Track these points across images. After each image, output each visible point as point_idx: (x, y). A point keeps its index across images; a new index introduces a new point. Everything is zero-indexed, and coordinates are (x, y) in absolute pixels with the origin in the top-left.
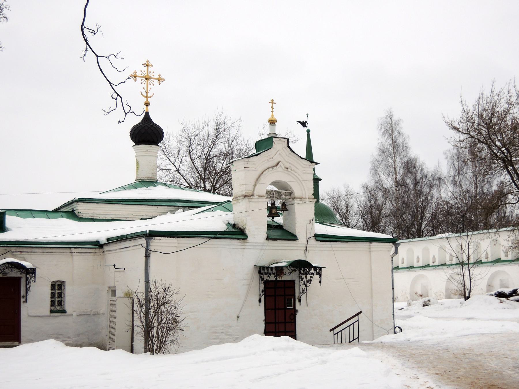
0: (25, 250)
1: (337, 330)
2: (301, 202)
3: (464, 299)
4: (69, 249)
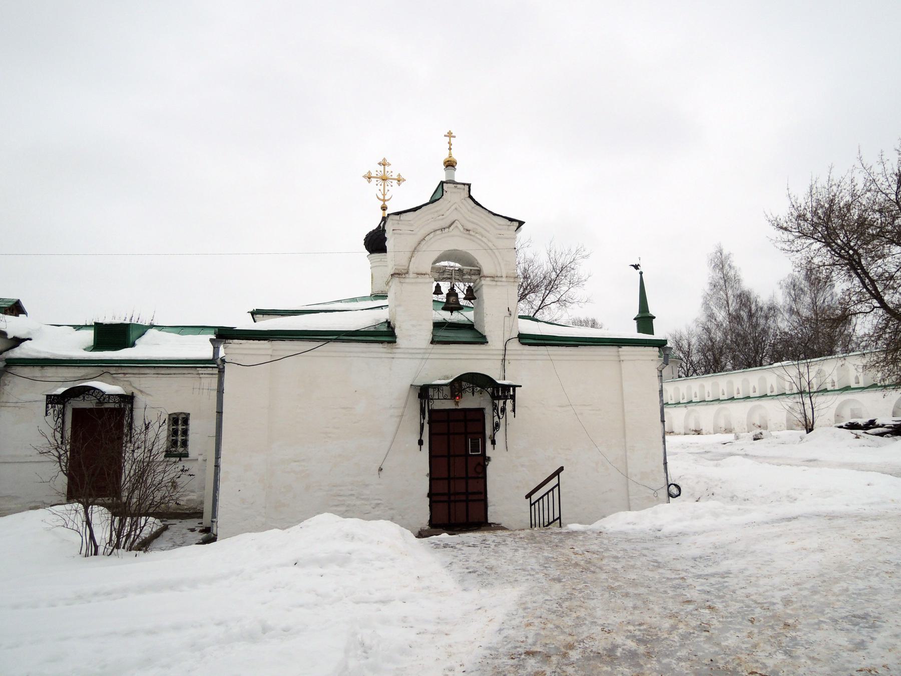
0: (130, 371)
1: (535, 497)
2: (494, 283)
3: (805, 431)
4: (194, 369)
